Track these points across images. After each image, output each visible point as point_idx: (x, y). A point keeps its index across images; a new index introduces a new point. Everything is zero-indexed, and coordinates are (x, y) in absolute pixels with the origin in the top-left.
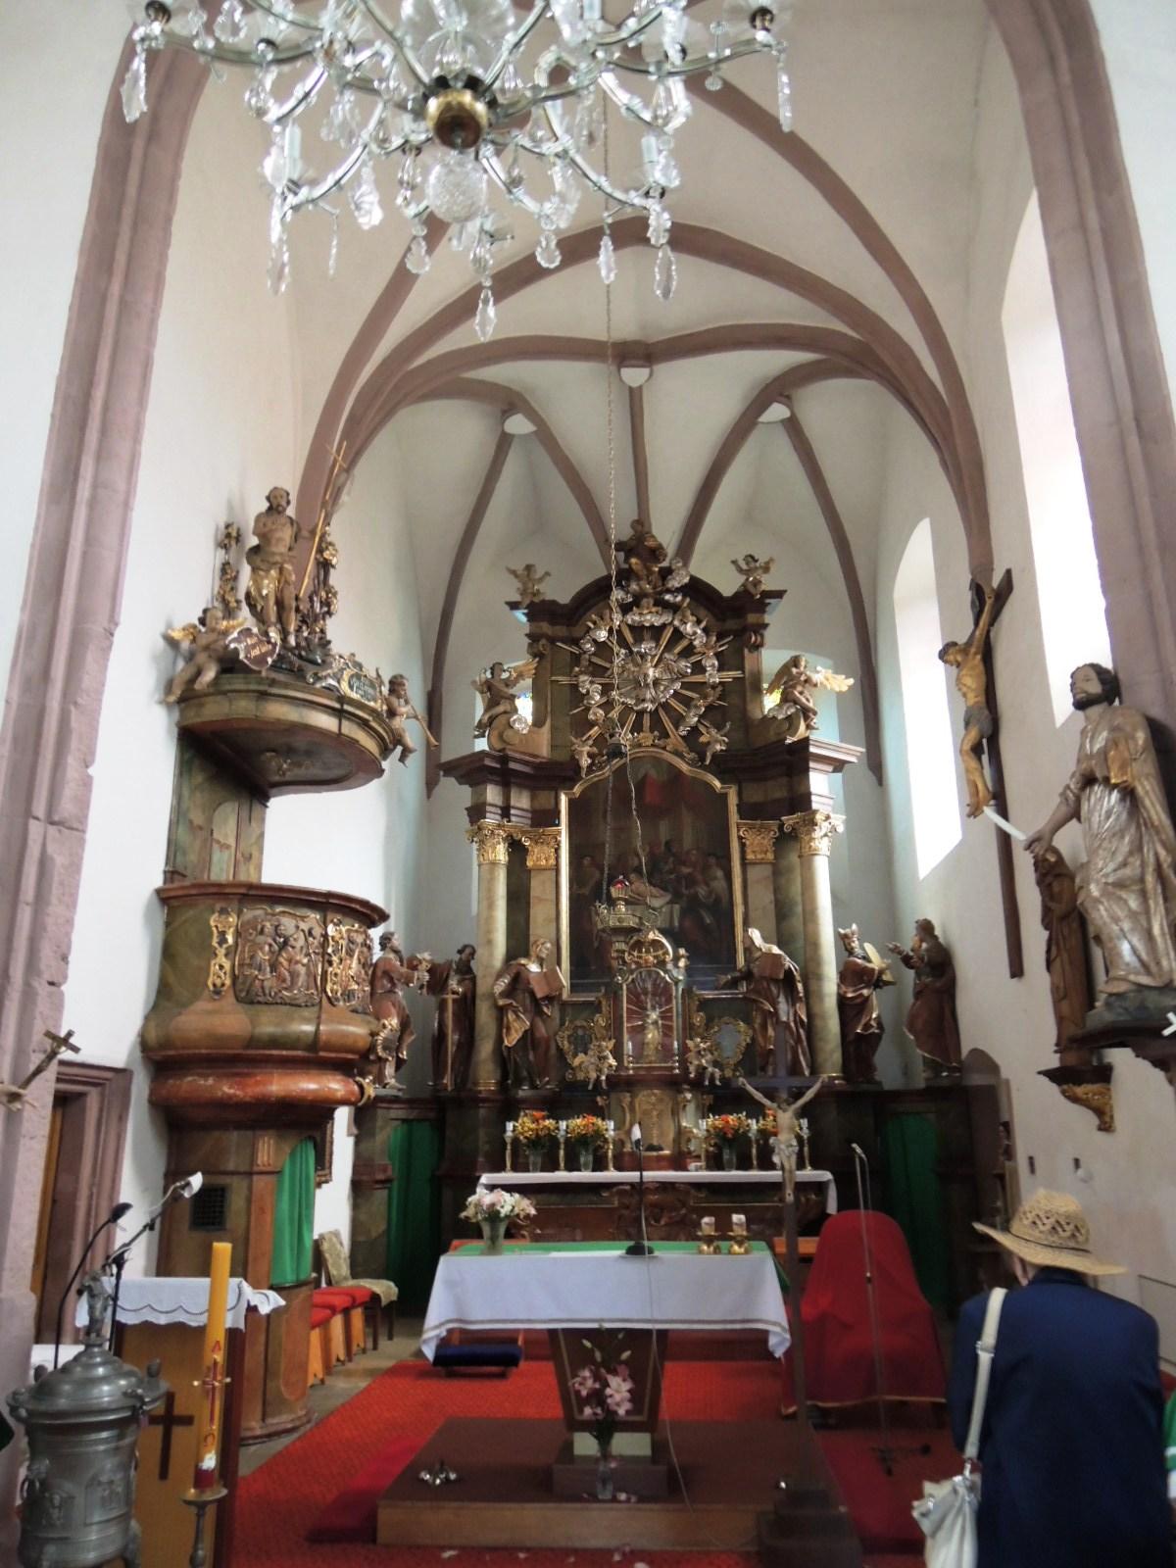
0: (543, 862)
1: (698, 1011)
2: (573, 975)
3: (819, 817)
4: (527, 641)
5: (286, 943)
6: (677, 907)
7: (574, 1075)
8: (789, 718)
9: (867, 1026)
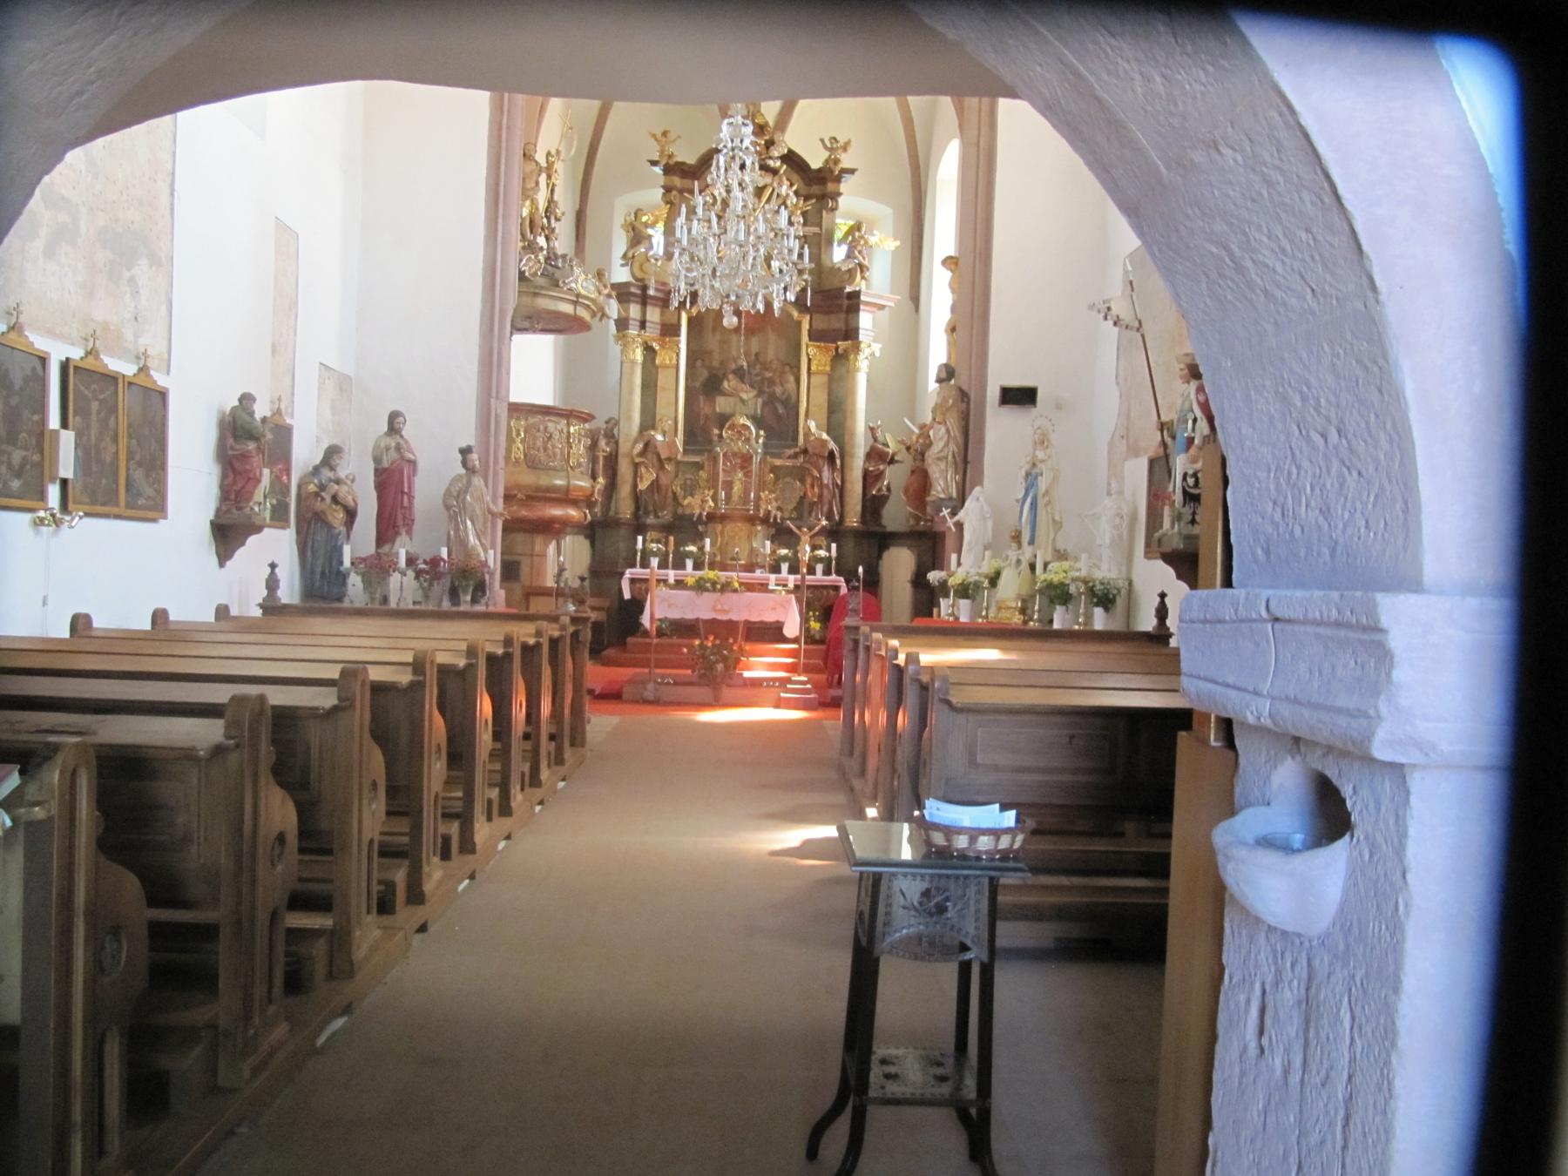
3: (862, 346)
4: (662, 191)
5: (551, 436)
6: (760, 400)
8: (849, 271)
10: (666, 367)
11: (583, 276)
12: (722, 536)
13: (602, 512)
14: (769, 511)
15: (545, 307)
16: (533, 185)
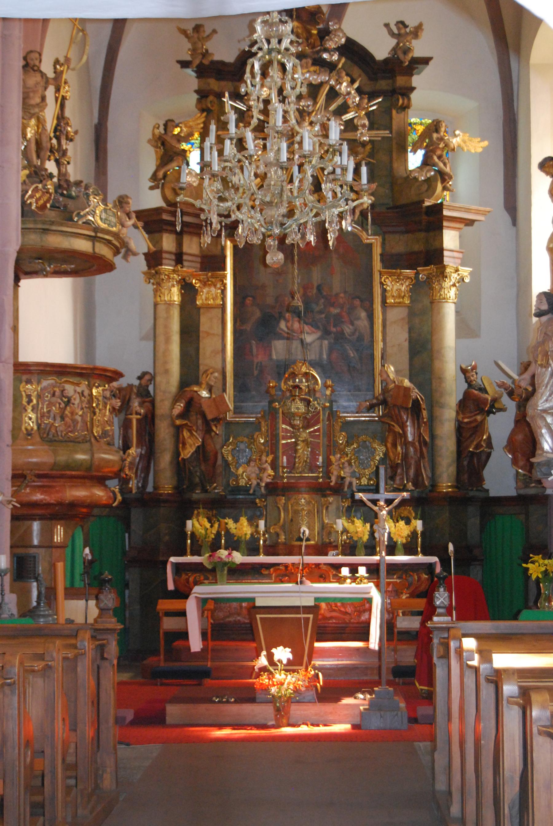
0: (211, 302)
1: (341, 431)
2: (236, 399)
3: (448, 270)
4: (195, 96)
5: (69, 401)
6: (326, 342)
7: (237, 481)
8: (428, 181)
9: (478, 446)
10: (209, 308)
11: (102, 207)
12: (286, 510)
13: (138, 488)
14: (343, 478)
15: (57, 245)
16: (38, 100)
